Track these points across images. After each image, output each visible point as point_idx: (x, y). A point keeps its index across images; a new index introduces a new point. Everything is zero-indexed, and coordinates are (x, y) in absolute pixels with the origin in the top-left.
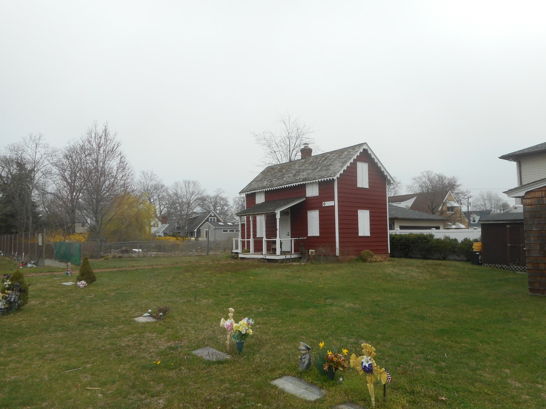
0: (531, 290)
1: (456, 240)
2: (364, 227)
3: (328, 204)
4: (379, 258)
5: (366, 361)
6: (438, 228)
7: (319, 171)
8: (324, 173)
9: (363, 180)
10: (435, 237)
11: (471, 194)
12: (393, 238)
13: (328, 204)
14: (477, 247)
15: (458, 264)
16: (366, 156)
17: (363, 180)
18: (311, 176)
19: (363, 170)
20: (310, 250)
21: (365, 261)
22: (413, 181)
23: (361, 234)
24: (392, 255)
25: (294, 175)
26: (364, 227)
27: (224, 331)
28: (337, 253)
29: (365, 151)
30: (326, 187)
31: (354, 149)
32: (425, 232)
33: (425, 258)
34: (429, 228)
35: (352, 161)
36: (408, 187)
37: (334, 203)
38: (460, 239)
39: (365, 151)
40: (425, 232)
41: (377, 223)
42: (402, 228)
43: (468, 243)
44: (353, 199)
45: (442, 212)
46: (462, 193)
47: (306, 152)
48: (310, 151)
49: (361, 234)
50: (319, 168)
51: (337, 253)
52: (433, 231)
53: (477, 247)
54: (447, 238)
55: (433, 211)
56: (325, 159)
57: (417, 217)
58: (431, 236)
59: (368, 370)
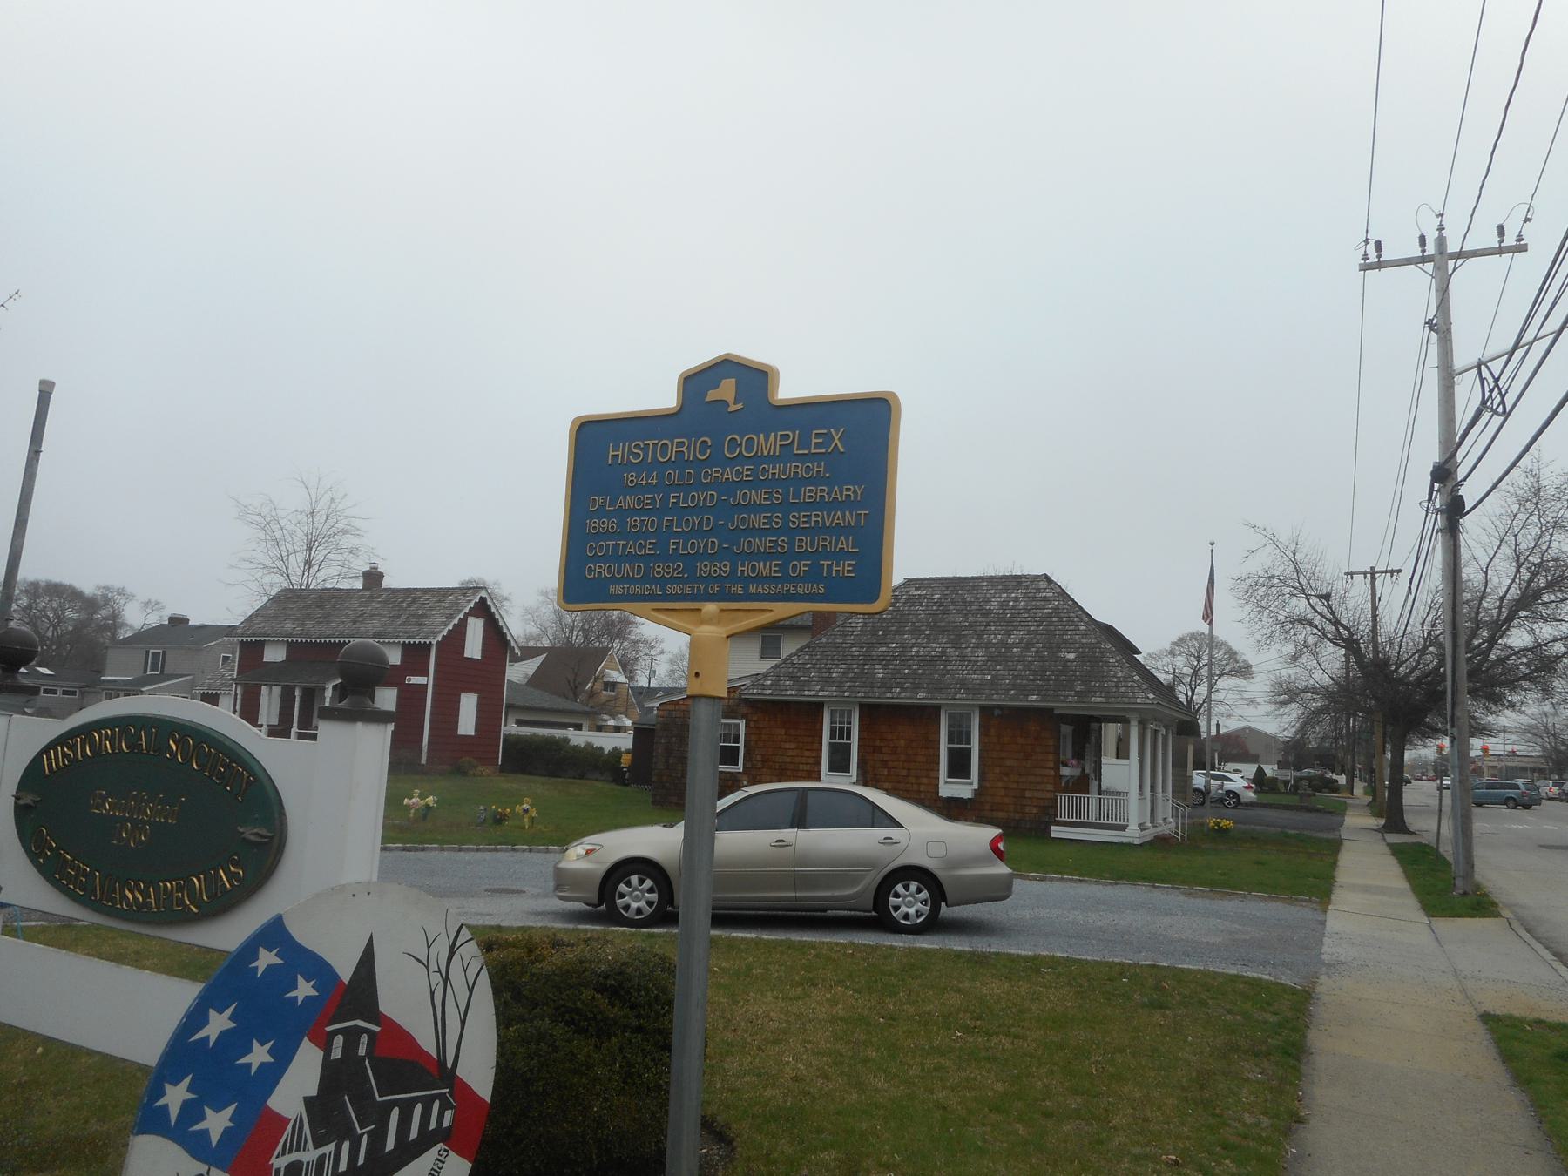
0: (654, 803)
1: (601, 749)
2: (467, 724)
3: (415, 680)
4: (487, 770)
5: (525, 806)
6: (578, 727)
7: (404, 623)
8: (415, 630)
9: (473, 647)
10: (386, 583)
11: (664, 646)
12: (507, 738)
13: (415, 680)
14: (626, 760)
15: (600, 785)
16: (483, 609)
17: (473, 647)
18: (390, 630)
19: (475, 631)
20: (742, 723)
21: (464, 774)
22: (541, 598)
23: (461, 732)
24: (503, 769)
25: (354, 622)
26: (467, 724)
27: (409, 807)
28: (424, 761)
29: (483, 600)
30: (415, 655)
31: (465, 595)
32: (558, 733)
33: (552, 774)
34: (565, 726)
35: (461, 616)
36: (527, 612)
37: (428, 681)
38: (608, 748)
39: (483, 600)
40: (558, 733)
41: (488, 717)
42: (520, 723)
43: (616, 753)
44: (458, 674)
45: (592, 694)
46: (646, 642)
47: (373, 577)
48: (381, 576)
49: (461, 732)
50: (403, 618)
51: (424, 761)
52: (570, 733)
53: (626, 760)
54: (589, 745)
55: (575, 690)
56: (414, 602)
57: (547, 705)
58: (567, 740)
59: (526, 811)
